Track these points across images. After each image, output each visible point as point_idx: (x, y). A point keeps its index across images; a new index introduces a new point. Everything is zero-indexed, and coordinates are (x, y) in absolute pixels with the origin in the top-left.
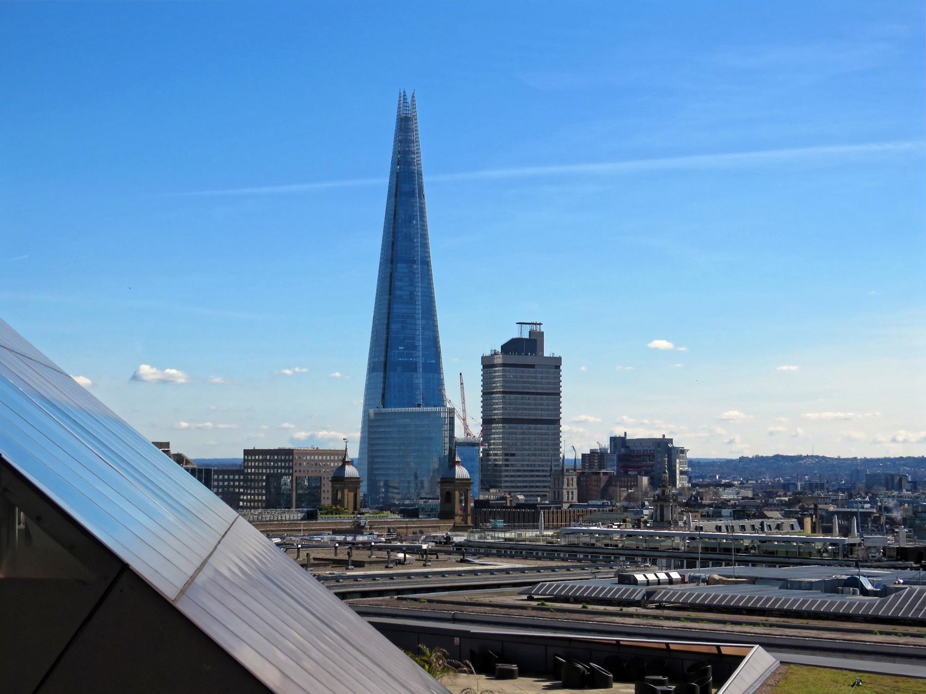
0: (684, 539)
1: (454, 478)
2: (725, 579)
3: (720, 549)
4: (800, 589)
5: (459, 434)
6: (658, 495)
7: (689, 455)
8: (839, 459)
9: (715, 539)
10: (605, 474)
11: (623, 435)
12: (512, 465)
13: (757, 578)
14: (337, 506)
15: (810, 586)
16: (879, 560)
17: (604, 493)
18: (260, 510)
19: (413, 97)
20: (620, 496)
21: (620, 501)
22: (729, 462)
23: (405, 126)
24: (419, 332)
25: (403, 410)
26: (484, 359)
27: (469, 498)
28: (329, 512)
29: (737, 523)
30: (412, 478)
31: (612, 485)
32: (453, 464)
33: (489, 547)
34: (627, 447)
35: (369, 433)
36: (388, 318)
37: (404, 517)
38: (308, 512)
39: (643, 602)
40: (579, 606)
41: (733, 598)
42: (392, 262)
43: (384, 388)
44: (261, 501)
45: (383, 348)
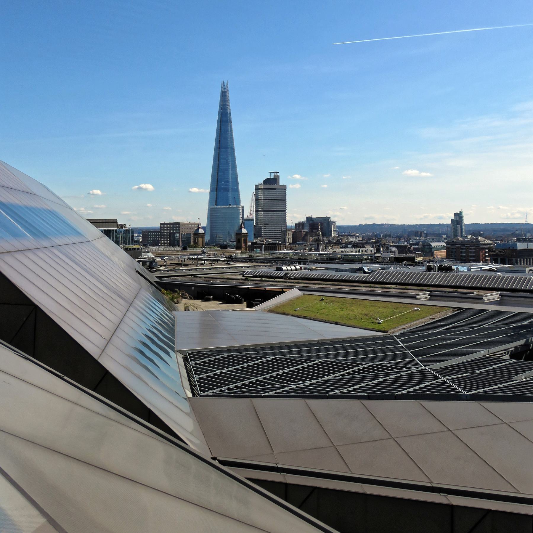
7: (337, 224)
8: (398, 225)
14: (196, 245)
15: (346, 270)
16: (388, 262)
17: (304, 239)
22: (355, 226)
23: (224, 95)
26: (256, 186)
27: (248, 240)
28: (192, 247)
29: (354, 250)
30: (227, 233)
41: (316, 275)
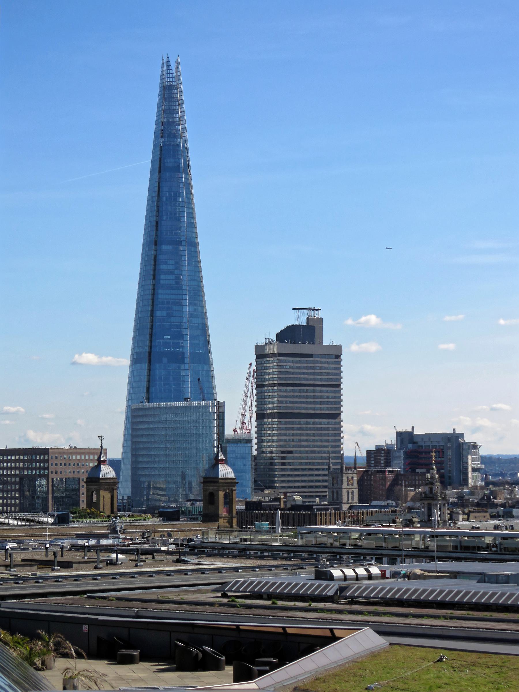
0: (425, 537)
1: (217, 478)
2: (426, 573)
3: (461, 547)
4: (497, 583)
5: (229, 432)
6: (425, 493)
7: (483, 452)
9: (456, 536)
10: (391, 472)
11: (410, 430)
12: (289, 464)
13: (458, 573)
14: (93, 510)
17: (390, 493)
18: (5, 515)
19: (177, 63)
20: (406, 496)
21: (406, 502)
23: (169, 96)
24: (187, 320)
25: (173, 404)
28: (82, 515)
30: (179, 479)
31: (397, 484)
32: (217, 462)
33: (223, 548)
34: (414, 443)
35: (133, 429)
36: (153, 305)
37: (164, 520)
38: (58, 516)
39: (336, 598)
40: (268, 603)
42: (156, 243)
43: (149, 381)
44: (15, 505)
45: (148, 337)
